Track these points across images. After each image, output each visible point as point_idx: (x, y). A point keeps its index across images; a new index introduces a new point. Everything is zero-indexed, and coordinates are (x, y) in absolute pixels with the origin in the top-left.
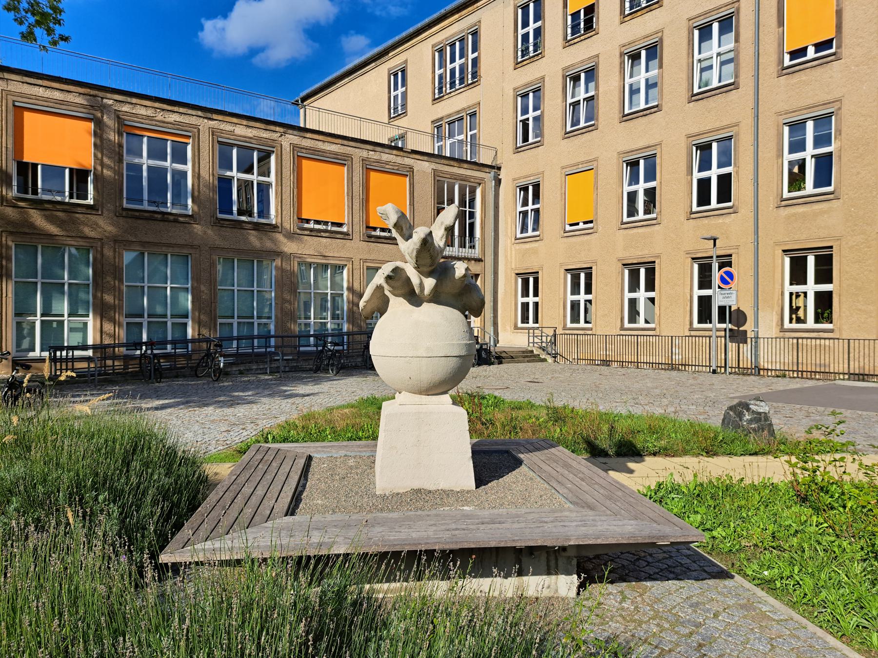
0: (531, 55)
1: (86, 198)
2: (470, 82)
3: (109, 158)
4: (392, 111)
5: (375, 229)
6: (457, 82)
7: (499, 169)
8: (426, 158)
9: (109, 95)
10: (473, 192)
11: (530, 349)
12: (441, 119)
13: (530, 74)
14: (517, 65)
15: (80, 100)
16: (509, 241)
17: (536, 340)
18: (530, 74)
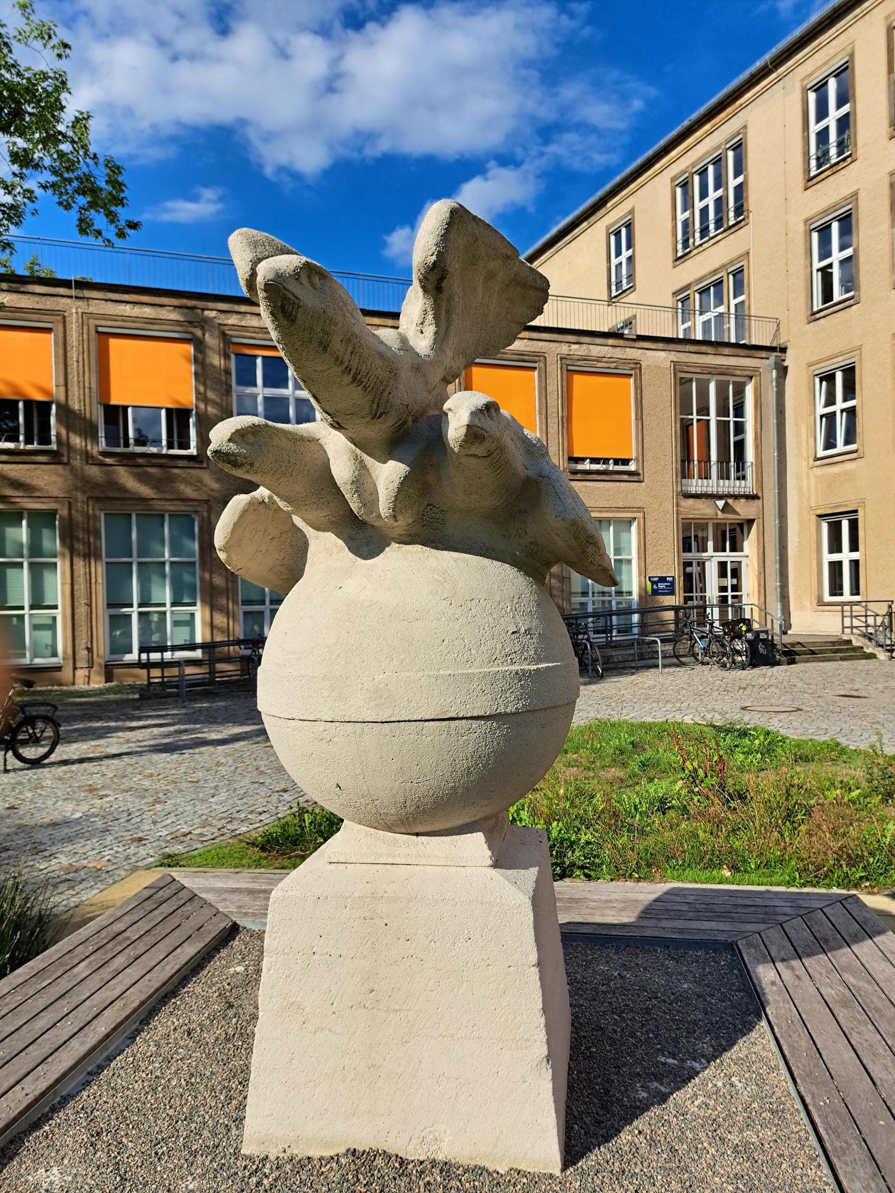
0: (833, 161)
1: (188, 447)
2: (731, 223)
3: (214, 390)
4: (613, 288)
5: (583, 460)
6: (712, 227)
7: (784, 350)
8: (660, 346)
9: (211, 305)
10: (740, 392)
11: (845, 637)
12: (688, 287)
13: (832, 192)
14: (810, 181)
15: (174, 316)
16: (804, 464)
17: (856, 623)
18: (832, 192)
